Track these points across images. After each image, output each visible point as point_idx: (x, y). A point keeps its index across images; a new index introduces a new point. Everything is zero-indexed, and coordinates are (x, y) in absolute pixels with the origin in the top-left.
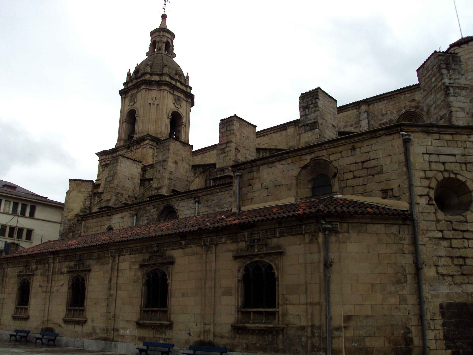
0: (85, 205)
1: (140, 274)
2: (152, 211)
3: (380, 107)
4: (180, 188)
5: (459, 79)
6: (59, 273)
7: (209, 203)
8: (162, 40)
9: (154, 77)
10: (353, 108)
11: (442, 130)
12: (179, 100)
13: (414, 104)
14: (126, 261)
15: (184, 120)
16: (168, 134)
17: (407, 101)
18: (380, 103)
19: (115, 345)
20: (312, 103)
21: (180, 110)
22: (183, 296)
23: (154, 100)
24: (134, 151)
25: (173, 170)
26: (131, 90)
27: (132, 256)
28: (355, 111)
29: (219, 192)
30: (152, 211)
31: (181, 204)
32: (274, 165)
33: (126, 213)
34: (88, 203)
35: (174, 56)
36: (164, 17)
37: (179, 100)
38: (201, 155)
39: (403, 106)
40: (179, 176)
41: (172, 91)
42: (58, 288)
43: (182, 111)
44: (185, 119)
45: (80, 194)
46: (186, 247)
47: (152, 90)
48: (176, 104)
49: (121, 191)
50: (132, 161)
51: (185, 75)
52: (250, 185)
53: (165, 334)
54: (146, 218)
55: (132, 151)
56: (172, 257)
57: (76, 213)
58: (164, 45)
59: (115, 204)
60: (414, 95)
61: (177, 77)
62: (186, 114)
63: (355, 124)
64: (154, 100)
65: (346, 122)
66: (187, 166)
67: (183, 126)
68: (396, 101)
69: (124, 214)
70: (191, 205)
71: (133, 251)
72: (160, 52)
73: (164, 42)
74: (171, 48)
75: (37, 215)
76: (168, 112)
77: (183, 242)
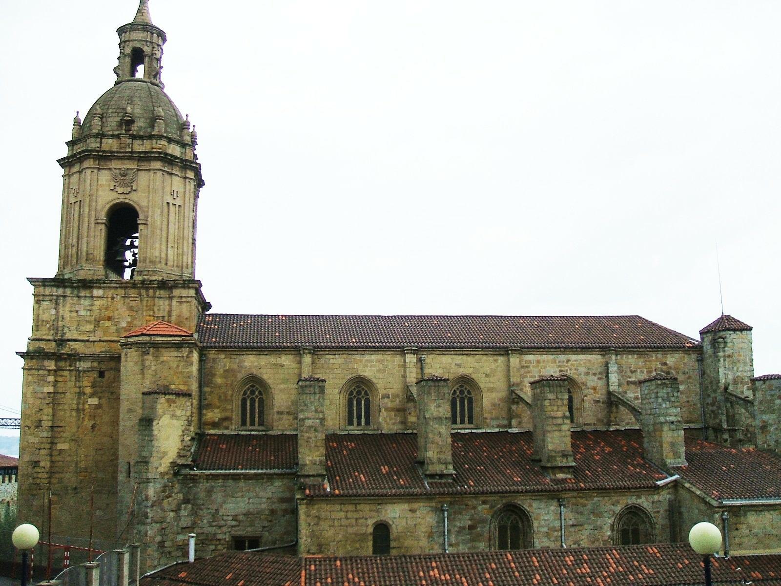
0: (184, 444)
2: (480, 508)
3: (629, 361)
7: (581, 509)
8: (140, 46)
9: (172, 146)
13: (665, 368)
17: (658, 363)
18: (630, 357)
20: (673, 396)
28: (600, 356)
30: (480, 508)
31: (535, 504)
33: (422, 504)
38: (345, 356)
39: (654, 367)
45: (175, 421)
52: (737, 529)
54: (468, 517)
57: (171, 460)
63: (599, 374)
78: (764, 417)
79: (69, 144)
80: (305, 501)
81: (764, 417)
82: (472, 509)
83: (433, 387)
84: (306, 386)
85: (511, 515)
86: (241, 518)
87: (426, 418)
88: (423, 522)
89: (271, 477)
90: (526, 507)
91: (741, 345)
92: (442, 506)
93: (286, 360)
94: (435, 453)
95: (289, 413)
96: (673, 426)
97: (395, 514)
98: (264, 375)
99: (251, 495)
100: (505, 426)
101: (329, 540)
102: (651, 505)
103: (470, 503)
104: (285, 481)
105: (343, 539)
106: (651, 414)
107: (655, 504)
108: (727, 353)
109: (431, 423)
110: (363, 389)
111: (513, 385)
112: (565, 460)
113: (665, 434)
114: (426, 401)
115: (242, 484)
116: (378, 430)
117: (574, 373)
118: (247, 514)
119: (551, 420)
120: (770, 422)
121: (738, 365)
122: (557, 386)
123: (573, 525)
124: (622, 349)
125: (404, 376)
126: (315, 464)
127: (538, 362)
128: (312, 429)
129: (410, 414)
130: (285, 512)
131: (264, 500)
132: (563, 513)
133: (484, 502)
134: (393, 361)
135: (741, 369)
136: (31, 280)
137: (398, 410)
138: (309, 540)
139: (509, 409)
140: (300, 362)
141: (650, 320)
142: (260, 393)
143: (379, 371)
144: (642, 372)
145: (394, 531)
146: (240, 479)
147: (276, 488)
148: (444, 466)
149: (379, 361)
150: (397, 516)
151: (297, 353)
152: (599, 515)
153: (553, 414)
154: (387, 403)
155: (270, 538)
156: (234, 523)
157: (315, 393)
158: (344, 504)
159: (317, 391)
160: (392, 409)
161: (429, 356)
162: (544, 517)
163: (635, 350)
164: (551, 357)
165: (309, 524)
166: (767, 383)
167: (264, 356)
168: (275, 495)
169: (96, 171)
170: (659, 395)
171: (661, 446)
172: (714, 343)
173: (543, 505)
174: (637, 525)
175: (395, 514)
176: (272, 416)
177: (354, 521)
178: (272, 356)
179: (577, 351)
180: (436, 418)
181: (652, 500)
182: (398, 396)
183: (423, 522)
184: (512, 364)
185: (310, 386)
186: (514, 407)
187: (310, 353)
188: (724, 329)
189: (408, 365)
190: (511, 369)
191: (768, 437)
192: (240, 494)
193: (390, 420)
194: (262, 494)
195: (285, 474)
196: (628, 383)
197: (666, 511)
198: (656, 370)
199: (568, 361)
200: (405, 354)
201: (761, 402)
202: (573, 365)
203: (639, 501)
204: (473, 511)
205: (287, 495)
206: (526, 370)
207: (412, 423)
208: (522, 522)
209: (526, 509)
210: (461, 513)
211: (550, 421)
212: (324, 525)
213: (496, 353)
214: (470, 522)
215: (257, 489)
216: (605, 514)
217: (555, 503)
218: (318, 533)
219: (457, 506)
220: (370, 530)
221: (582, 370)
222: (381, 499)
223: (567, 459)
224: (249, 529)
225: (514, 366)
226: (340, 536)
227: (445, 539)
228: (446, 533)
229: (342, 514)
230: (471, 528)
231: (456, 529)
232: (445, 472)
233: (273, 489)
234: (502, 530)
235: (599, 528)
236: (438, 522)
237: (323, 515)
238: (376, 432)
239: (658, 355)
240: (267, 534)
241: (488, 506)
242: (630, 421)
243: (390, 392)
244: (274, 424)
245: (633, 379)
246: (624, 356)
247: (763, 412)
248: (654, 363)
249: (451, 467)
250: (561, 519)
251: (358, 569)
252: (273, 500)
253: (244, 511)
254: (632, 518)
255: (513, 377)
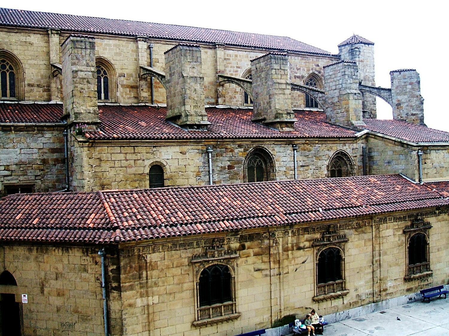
1: (403, 238)
2: (236, 151)
3: (296, 61)
6: (295, 248)
7: (307, 153)
13: (318, 68)
14: (389, 228)
18: (296, 58)
19: (387, 303)
22: (438, 250)
27: (395, 223)
29: (318, 144)
30: (236, 151)
31: (277, 149)
32: (439, 151)
33: (190, 147)
42: (297, 266)
46: (439, 215)
52: (425, 163)
53: (427, 280)
54: (227, 159)
56: (429, 223)
68: (307, 61)
70: (289, 152)
71: (396, 219)
77: (437, 212)
78: (399, 98)
80: (87, 144)
81: (399, 98)
82: (230, 152)
83: (189, 51)
84: (77, 41)
85: (257, 158)
86: (14, 167)
87: (183, 77)
88: (191, 163)
89: (41, 130)
90: (270, 151)
91: (368, 55)
92: (207, 149)
93: (36, 39)
94: (192, 107)
95: (38, 86)
96: (355, 97)
97: (169, 156)
98: (15, 51)
99: (23, 146)
100: (213, 104)
101: (111, 180)
102: (352, 151)
103: (229, 147)
104: (55, 133)
105: (123, 179)
106: (335, 89)
107: (354, 151)
108: (360, 59)
109: (189, 81)
110: (102, 69)
111: (219, 72)
112: (289, 117)
113: (350, 102)
114: (183, 62)
115: (12, 135)
116: (116, 103)
118: (19, 164)
119: (277, 84)
120: (403, 101)
121: (367, 68)
122: (280, 59)
123: (302, 166)
124: (292, 52)
125: (137, 60)
126: (90, 113)
127: (236, 56)
128: (85, 81)
129: (142, 90)
130: (57, 161)
131: (36, 150)
132: (295, 156)
133: (240, 146)
134: (128, 46)
135: (368, 71)
137: (132, 87)
138: (92, 180)
139: (216, 91)
140: (48, 42)
142: (11, 68)
143: (116, 54)
144: (304, 70)
145: (168, 172)
146: (11, 130)
147: (47, 139)
148: (200, 118)
149: (115, 45)
150: (170, 158)
151: (45, 33)
152: (318, 158)
153: (279, 81)
154: (123, 81)
155: (43, 186)
156: (7, 173)
157: (86, 48)
158: (124, 147)
159: (88, 47)
160: (128, 86)
161: (156, 44)
162: (283, 157)
163: (300, 53)
165: (92, 166)
166: (402, 73)
167: (13, 34)
168: (47, 146)
170: (346, 73)
171: (347, 111)
172: (352, 52)
173: (282, 149)
174: (341, 167)
175: (169, 156)
176: (23, 88)
177: (132, 162)
178: (22, 34)
179: (262, 50)
180: (192, 77)
181: (353, 147)
182: (131, 75)
183: (191, 163)
184: (218, 56)
185: (82, 41)
186: (220, 89)
187: (57, 34)
188: (354, 45)
189: (140, 50)
190: (218, 59)
191: (401, 111)
192: (11, 145)
193: (126, 95)
194: (33, 145)
195: (56, 126)
196: (295, 77)
197: (361, 156)
198: (312, 69)
200: (137, 41)
201: (397, 87)
203: (345, 148)
204: (231, 153)
205: (57, 146)
206: (228, 61)
207: (144, 98)
208: (266, 164)
209: (270, 152)
210: (222, 156)
211: (277, 86)
212: (105, 166)
213: (208, 47)
214: (229, 163)
215: (28, 141)
216: (323, 158)
217: (290, 148)
218: (100, 174)
219: (218, 149)
220: (147, 170)
222: (157, 142)
223: (290, 116)
224: (21, 178)
225: (220, 57)
226: (121, 176)
227: (210, 178)
228: (211, 172)
229: (122, 157)
230: (230, 167)
231: (218, 168)
232: (202, 123)
233: (44, 140)
234: (250, 169)
235: (319, 168)
236: (204, 163)
237: (104, 157)
238: (115, 104)
239: (314, 59)
240: (39, 182)
241: (243, 149)
242: (296, 105)
243: (125, 72)
244: (26, 95)
245: (298, 75)
246: (293, 57)
247: (398, 94)
248: (311, 64)
249: (206, 118)
250: (294, 161)
251: (156, 200)
252: (44, 150)
253: (16, 161)
254: (337, 162)
255: (220, 65)
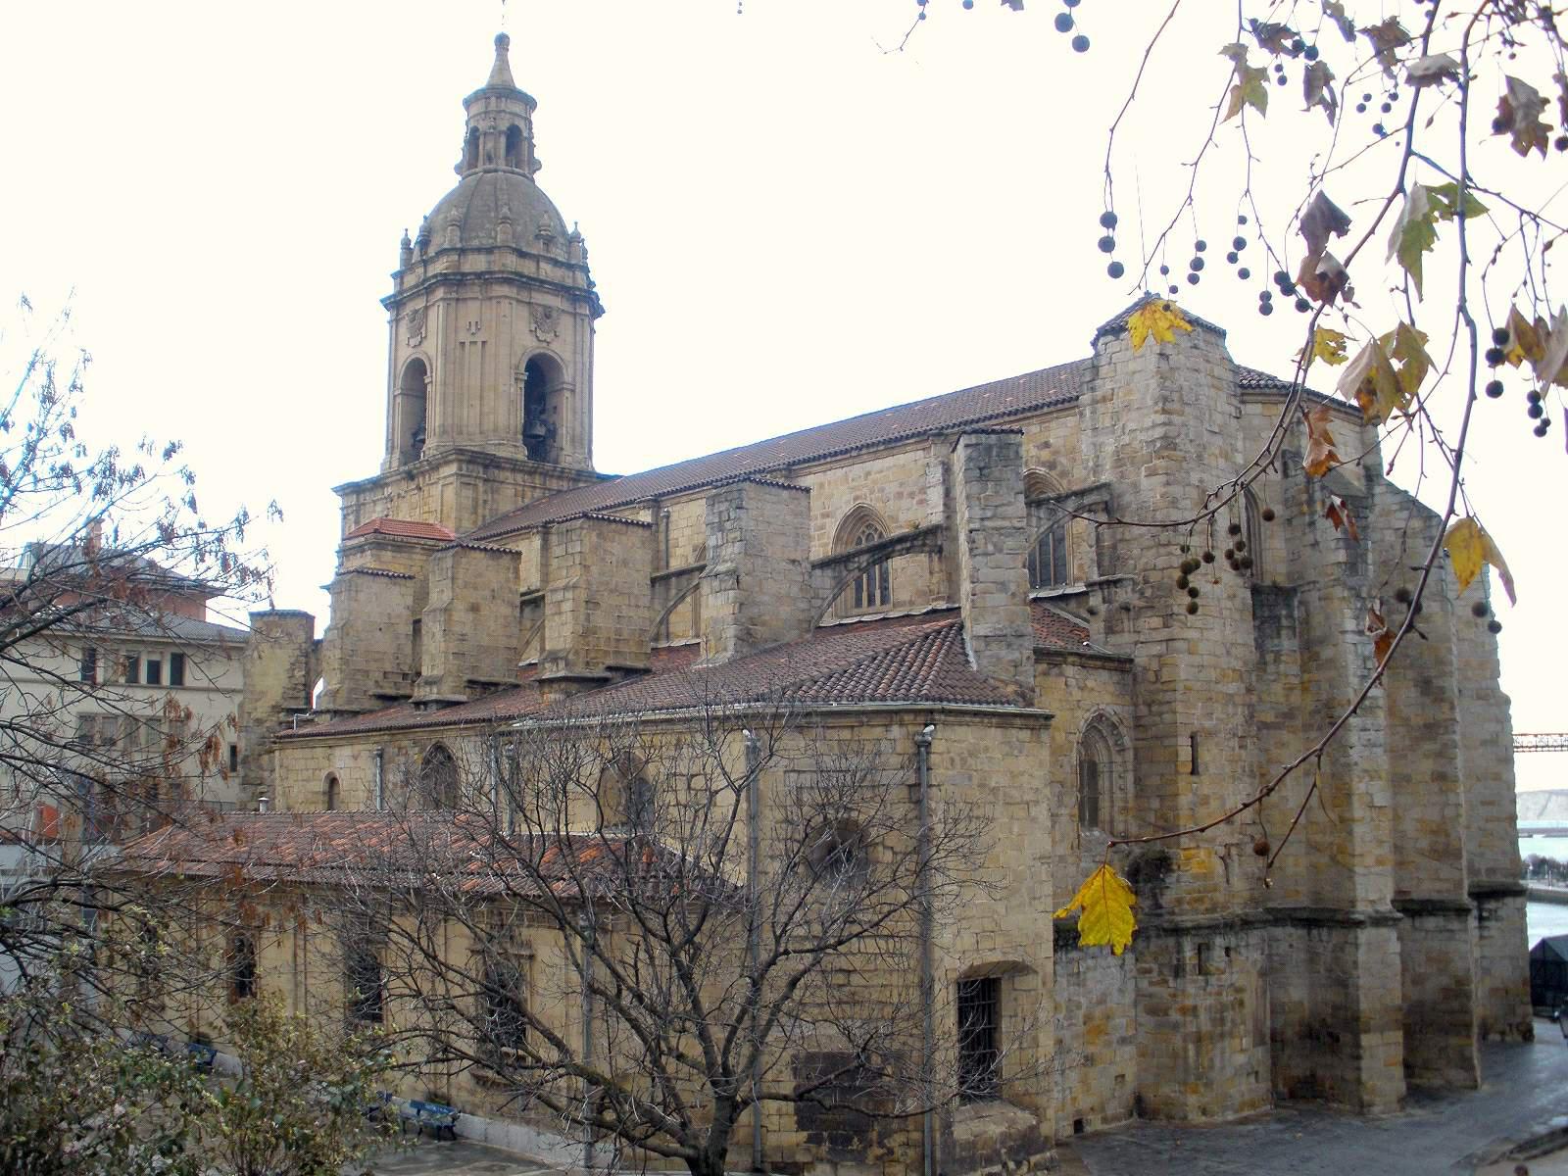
0: (294, 681)
4: (491, 670)
5: (1009, 504)
8: (501, 131)
10: (914, 447)
11: (831, 721)
12: (548, 316)
13: (1045, 455)
15: (567, 375)
16: (520, 428)
21: (553, 346)
23: (473, 330)
24: (426, 489)
25: (467, 630)
26: (412, 297)
34: (299, 674)
35: (535, 166)
36: (502, 42)
37: (548, 316)
40: (485, 641)
41: (524, 296)
43: (561, 349)
44: (570, 371)
47: (465, 299)
48: (539, 333)
49: (363, 666)
50: (386, 580)
51: (570, 230)
55: (419, 488)
58: (503, 140)
59: (350, 701)
60: (1048, 429)
61: (537, 249)
62: (575, 353)
64: (473, 330)
65: (901, 485)
66: (505, 610)
67: (567, 394)
69: (358, 748)
72: (492, 166)
73: (500, 133)
74: (525, 145)
75: (189, 680)
76: (514, 361)
79: (395, 276)
108: (1099, 394)
117: (877, 499)
136: (336, 490)
141: (943, 392)
164: (840, 472)
169: (453, 303)
199: (868, 474)
202: (875, 482)
221: (892, 488)
